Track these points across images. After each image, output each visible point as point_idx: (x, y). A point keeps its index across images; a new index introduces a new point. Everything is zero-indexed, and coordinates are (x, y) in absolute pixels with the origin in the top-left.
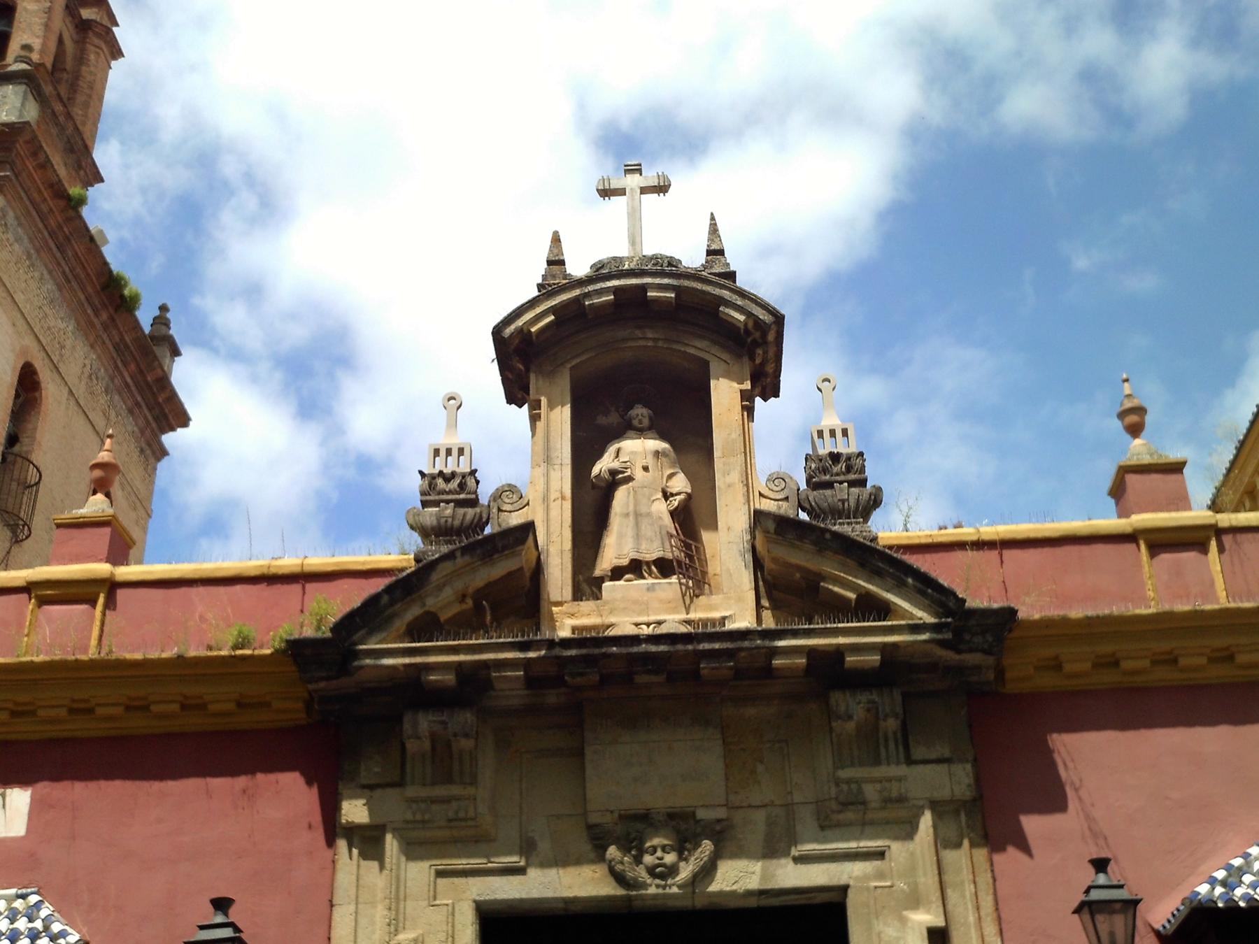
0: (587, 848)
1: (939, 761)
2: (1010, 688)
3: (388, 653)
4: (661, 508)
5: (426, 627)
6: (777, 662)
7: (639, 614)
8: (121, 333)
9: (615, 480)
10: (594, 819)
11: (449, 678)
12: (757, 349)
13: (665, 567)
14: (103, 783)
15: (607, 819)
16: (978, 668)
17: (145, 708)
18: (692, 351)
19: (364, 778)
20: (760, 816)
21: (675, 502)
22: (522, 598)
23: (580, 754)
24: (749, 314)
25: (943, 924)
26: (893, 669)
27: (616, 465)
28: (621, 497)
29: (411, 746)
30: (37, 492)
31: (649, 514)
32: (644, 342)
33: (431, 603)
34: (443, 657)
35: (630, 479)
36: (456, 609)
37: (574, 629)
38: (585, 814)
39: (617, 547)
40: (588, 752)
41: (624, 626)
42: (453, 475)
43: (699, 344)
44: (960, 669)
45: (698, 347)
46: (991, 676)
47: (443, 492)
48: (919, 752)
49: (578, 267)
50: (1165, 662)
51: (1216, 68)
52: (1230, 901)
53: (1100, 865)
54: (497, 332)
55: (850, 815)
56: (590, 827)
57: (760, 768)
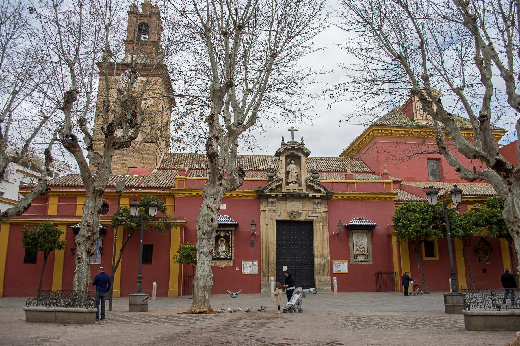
5: (271, 190)
6: (326, 209)
25: (256, 272)
26: (322, 197)
34: (273, 194)
45: (300, 154)
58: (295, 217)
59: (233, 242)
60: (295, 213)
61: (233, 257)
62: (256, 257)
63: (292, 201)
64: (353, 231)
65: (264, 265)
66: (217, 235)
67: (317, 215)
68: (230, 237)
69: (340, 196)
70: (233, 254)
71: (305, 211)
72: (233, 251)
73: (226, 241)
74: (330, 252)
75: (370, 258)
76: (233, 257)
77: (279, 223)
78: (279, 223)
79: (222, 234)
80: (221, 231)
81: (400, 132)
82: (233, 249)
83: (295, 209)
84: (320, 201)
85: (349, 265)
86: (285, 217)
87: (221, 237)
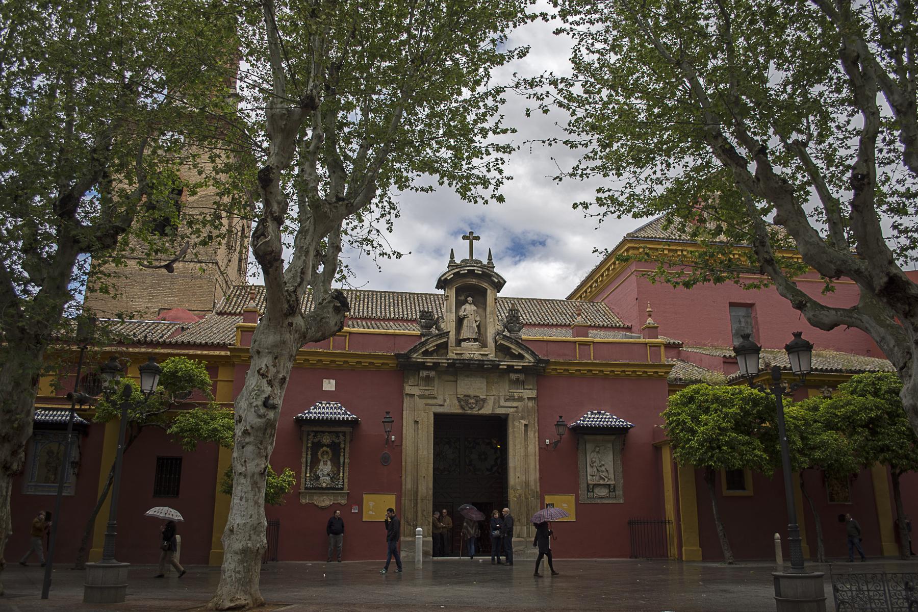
0: (856, 203)
3: (417, 357)
5: (426, 353)
6: (533, 394)
8: (808, 123)
9: (464, 317)
13: (475, 340)
15: (461, 397)
22: (443, 348)
23: (456, 381)
26: (525, 370)
34: (429, 361)
39: (465, 334)
41: (467, 356)
53: (561, 417)
58: (471, 408)
60: (473, 401)
61: (346, 487)
62: (393, 486)
63: (467, 376)
64: (586, 437)
65: (406, 501)
66: (316, 440)
67: (515, 404)
68: (342, 445)
69: (560, 369)
70: (346, 480)
71: (494, 399)
72: (346, 474)
73: (333, 455)
74: (540, 478)
75: (619, 492)
76: (346, 487)
77: (440, 419)
78: (440, 419)
79: (326, 440)
80: (323, 432)
81: (679, 253)
82: (346, 469)
83: (472, 393)
84: (521, 377)
85: (579, 506)
87: (323, 445)
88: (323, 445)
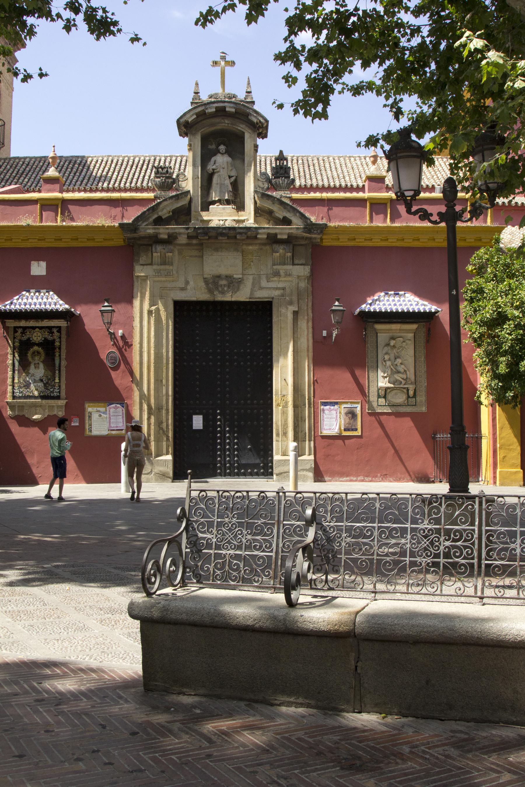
1: (301, 265)
2: (324, 244)
4: (228, 182)
5: (159, 221)
7: (221, 216)
10: (205, 276)
11: (166, 237)
12: (261, 129)
14: (88, 207)
16: (315, 238)
17: (419, 240)
18: (239, 128)
19: (141, 262)
20: (251, 277)
21: (233, 179)
23: (202, 257)
24: (149, 419)
27: (214, 167)
28: (386, 168)
29: (155, 254)
30: (4, 128)
31: (224, 184)
32: (225, 124)
33: (160, 214)
35: (218, 172)
36: (167, 215)
37: (90, 413)
38: (203, 275)
40: (204, 257)
42: (165, 168)
43: (241, 126)
44: (311, 238)
45: (241, 127)
46: (319, 241)
47: (161, 173)
48: (296, 262)
49: (204, 97)
50: (335, 239)
51: (465, 98)
52: (397, 309)
54: (178, 121)
55: (275, 279)
56: (204, 278)
57: (252, 264)
59: (63, 356)
66: (25, 338)
68: (57, 344)
72: (63, 379)
73: (47, 354)
75: (422, 398)
76: (63, 394)
83: (223, 271)
86: (196, 292)
88: (35, 344)
